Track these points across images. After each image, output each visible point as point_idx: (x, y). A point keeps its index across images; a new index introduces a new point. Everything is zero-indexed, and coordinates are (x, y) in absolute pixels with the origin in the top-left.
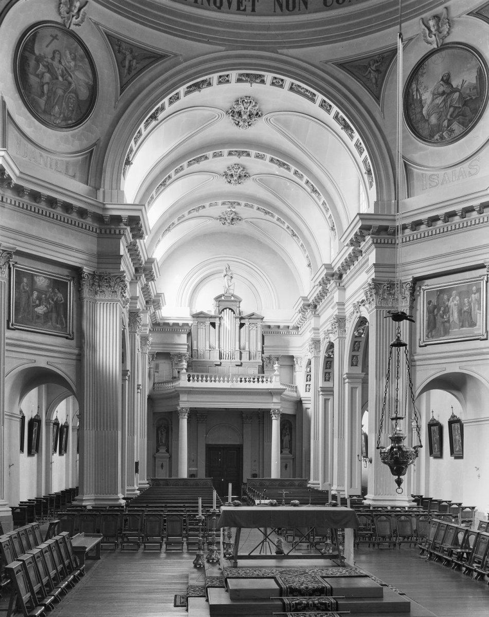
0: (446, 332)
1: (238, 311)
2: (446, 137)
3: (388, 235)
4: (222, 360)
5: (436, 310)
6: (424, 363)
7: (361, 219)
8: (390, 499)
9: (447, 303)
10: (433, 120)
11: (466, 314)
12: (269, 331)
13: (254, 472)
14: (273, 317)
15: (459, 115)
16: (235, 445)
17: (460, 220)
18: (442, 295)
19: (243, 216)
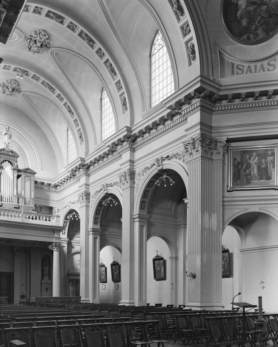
0: (248, 182)
1: (16, 164)
2: (252, 38)
3: (211, 102)
4: (3, 202)
5: (240, 166)
6: (231, 203)
7: (201, 81)
8: (209, 305)
9: (249, 161)
10: (244, 22)
11: (264, 170)
12: (39, 185)
13: (23, 294)
14: (41, 175)
15: (265, 24)
16: (7, 272)
17: (266, 100)
18: (244, 155)
19: (23, 88)
